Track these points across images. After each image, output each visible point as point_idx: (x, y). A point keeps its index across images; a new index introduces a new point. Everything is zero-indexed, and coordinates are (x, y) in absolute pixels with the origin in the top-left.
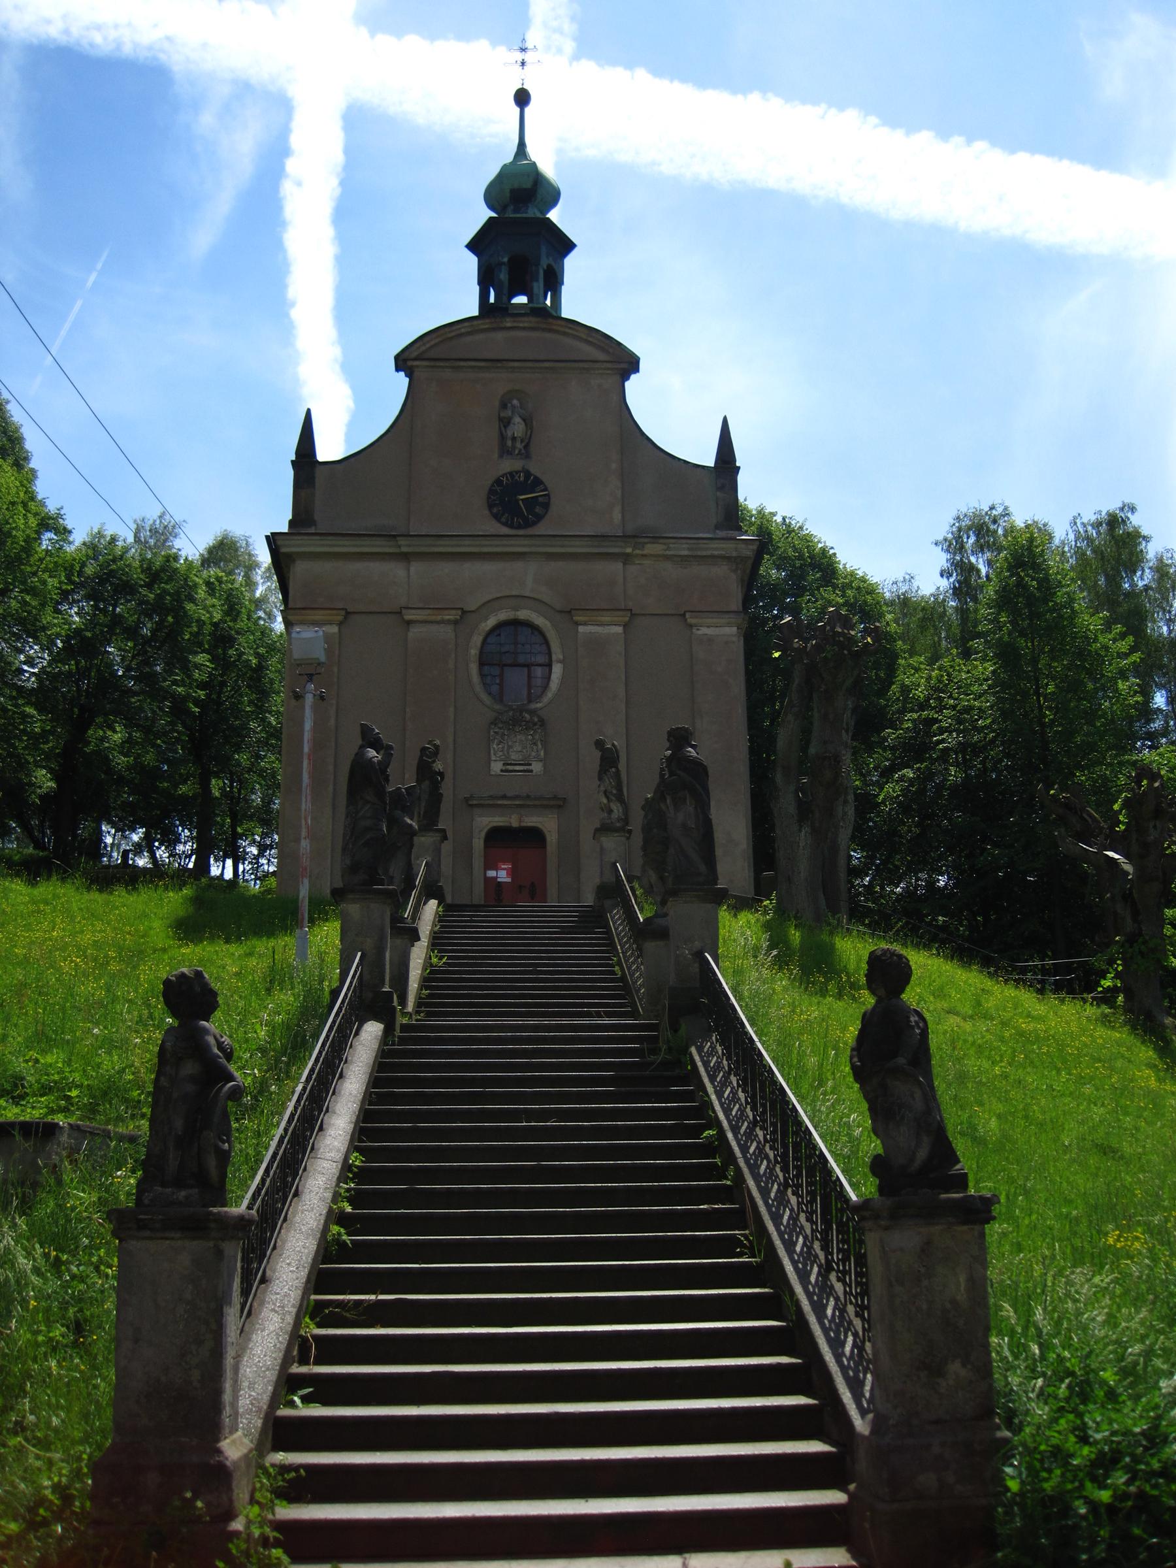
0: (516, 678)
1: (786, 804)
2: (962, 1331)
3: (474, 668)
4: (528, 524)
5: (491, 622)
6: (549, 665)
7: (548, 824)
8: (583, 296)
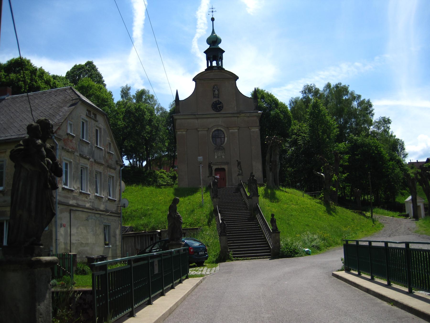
0: (218, 140)
1: (268, 168)
2: (278, 241)
3: (211, 139)
4: (219, 111)
5: (214, 130)
6: (224, 138)
7: (226, 167)
8: (228, 65)
